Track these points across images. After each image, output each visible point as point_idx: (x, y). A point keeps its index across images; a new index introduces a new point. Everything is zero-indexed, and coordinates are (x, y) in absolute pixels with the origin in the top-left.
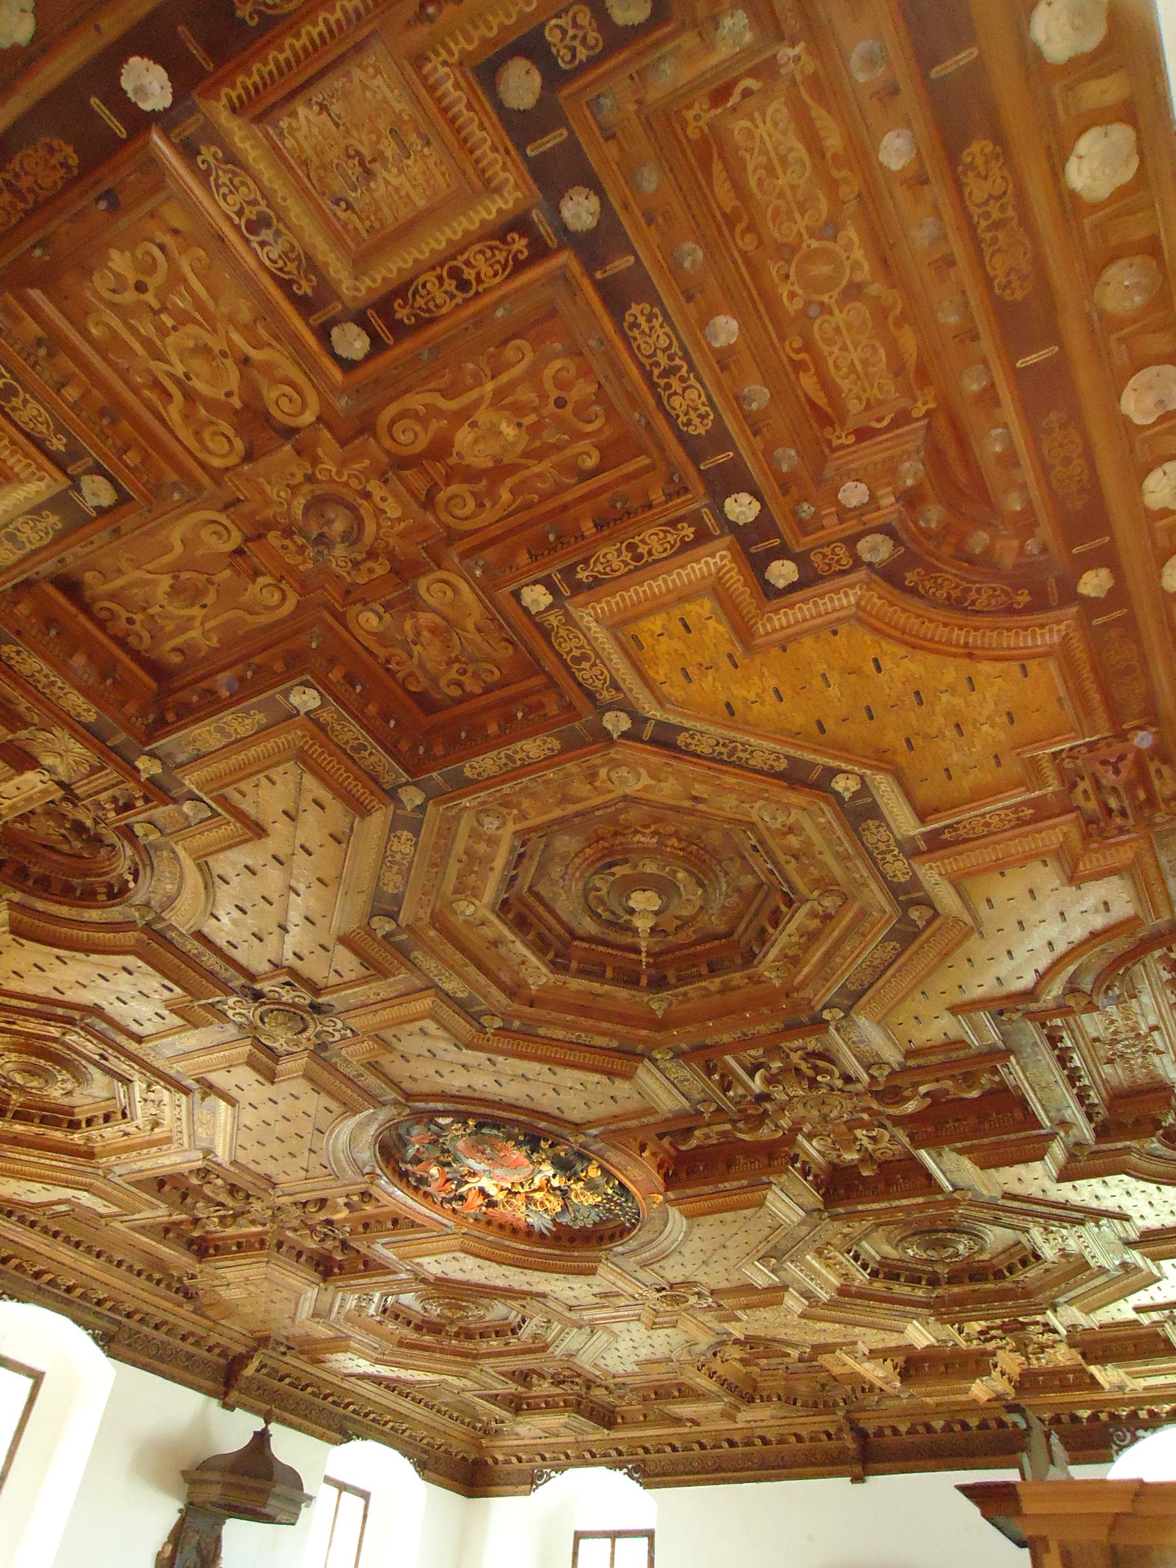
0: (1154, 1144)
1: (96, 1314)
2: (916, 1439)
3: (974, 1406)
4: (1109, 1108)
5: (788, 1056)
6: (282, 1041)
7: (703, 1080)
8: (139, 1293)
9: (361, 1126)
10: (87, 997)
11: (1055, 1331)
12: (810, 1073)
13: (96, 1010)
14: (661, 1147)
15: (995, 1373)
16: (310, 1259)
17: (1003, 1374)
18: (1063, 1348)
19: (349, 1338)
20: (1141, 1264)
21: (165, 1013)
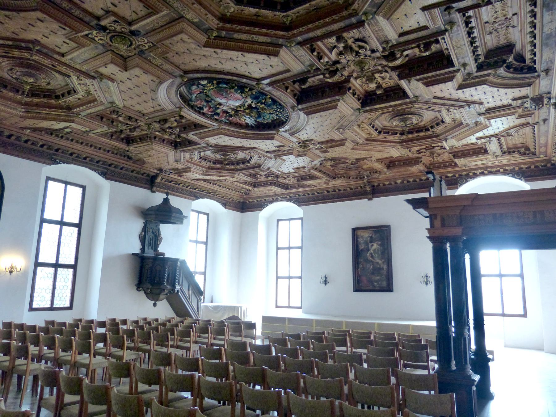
0: (501, 71)
1: (98, 166)
2: (390, 186)
3: (412, 175)
4: (486, 57)
5: (347, 41)
6: (124, 51)
8: (109, 158)
9: (169, 87)
10: (31, 36)
11: (445, 149)
12: (357, 49)
13: (35, 42)
14: (295, 88)
15: (421, 164)
16: (168, 142)
17: (423, 164)
18: (446, 154)
19: (190, 168)
20: (483, 121)
21: (68, 41)
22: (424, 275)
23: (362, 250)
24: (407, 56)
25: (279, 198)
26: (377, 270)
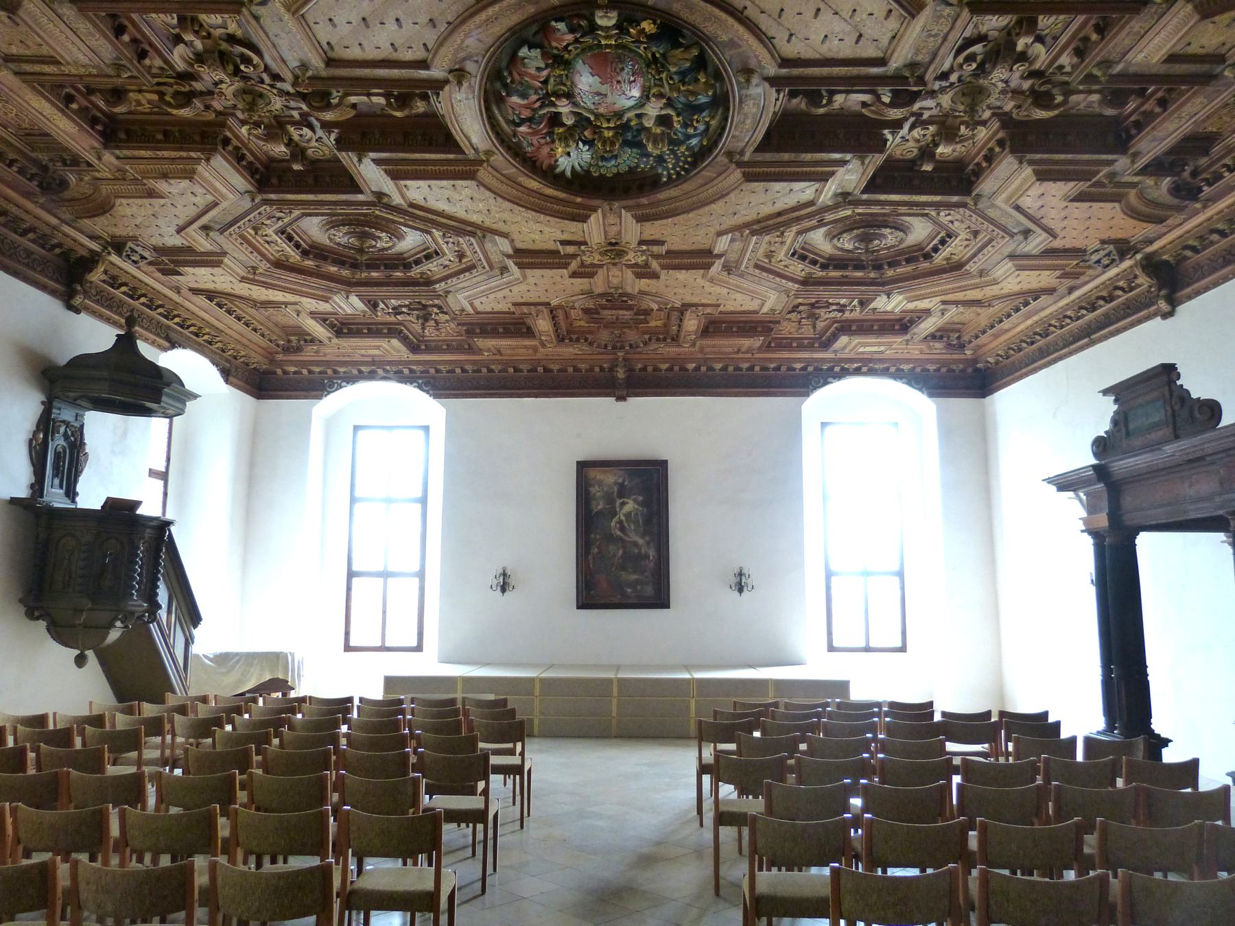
2: (670, 374)
7: (110, 41)
22: (737, 571)
23: (599, 513)
24: (354, 106)
25: (380, 372)
26: (633, 560)
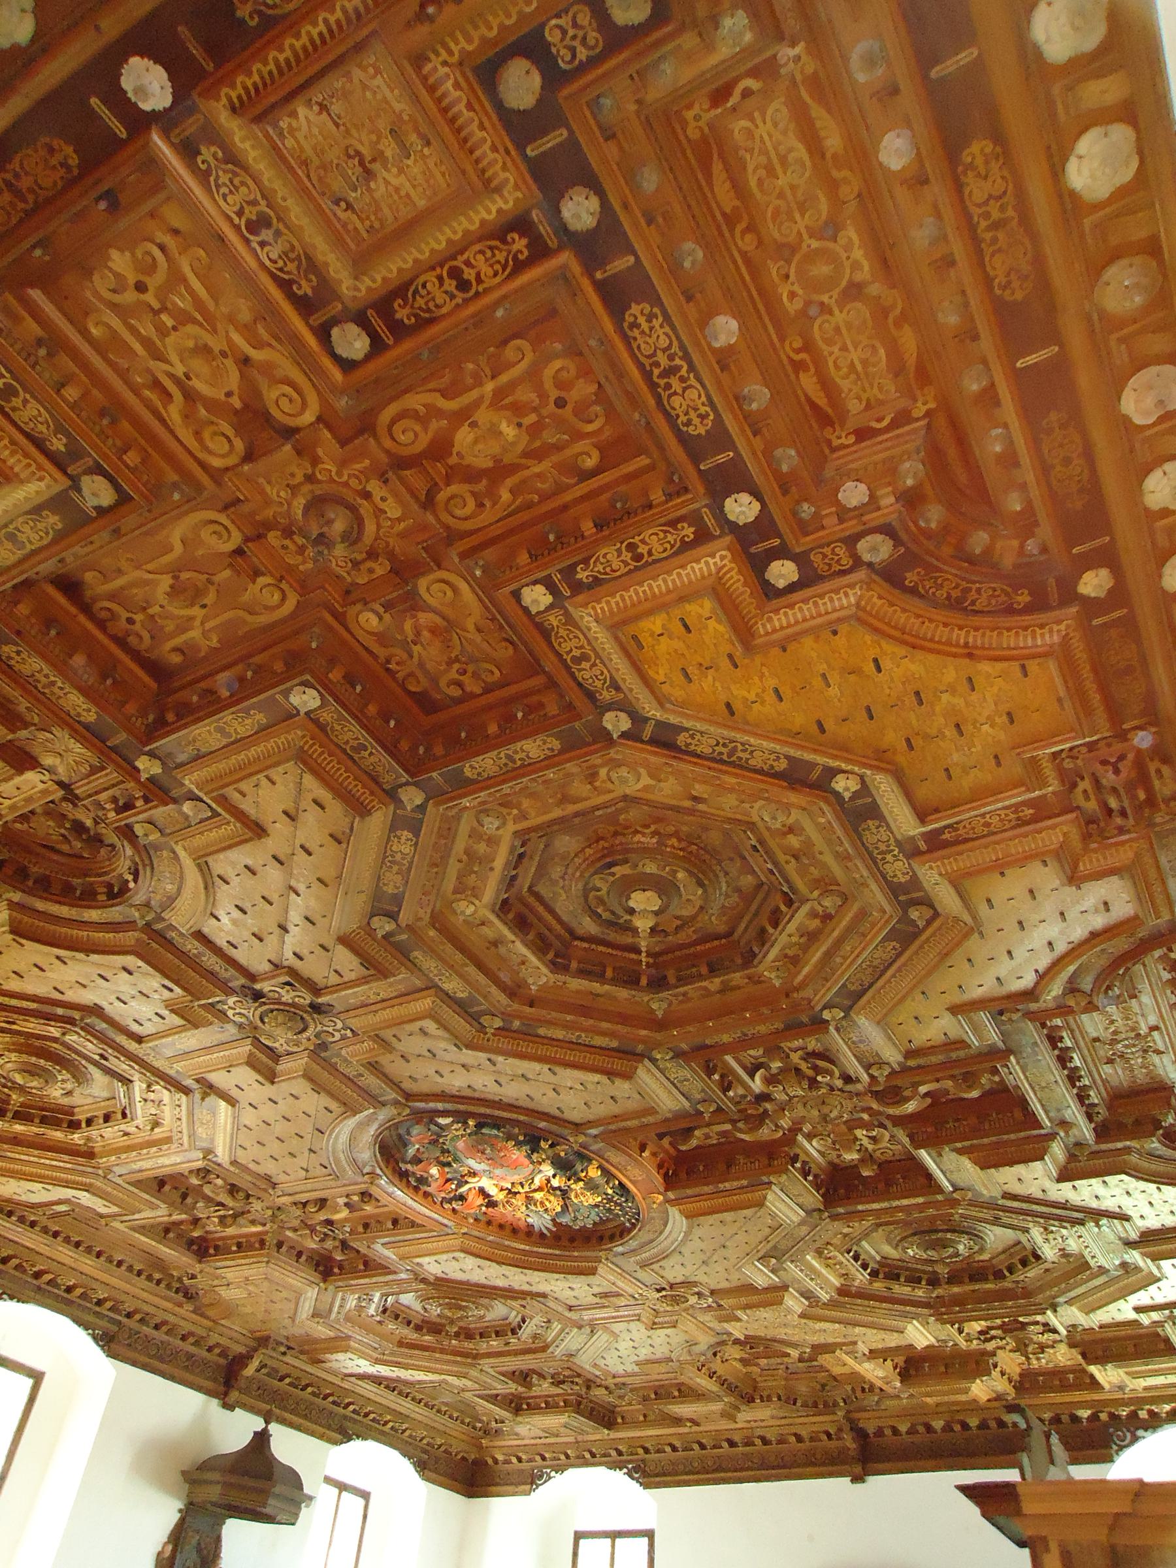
2: (916, 1439)
